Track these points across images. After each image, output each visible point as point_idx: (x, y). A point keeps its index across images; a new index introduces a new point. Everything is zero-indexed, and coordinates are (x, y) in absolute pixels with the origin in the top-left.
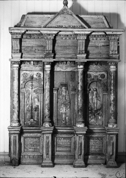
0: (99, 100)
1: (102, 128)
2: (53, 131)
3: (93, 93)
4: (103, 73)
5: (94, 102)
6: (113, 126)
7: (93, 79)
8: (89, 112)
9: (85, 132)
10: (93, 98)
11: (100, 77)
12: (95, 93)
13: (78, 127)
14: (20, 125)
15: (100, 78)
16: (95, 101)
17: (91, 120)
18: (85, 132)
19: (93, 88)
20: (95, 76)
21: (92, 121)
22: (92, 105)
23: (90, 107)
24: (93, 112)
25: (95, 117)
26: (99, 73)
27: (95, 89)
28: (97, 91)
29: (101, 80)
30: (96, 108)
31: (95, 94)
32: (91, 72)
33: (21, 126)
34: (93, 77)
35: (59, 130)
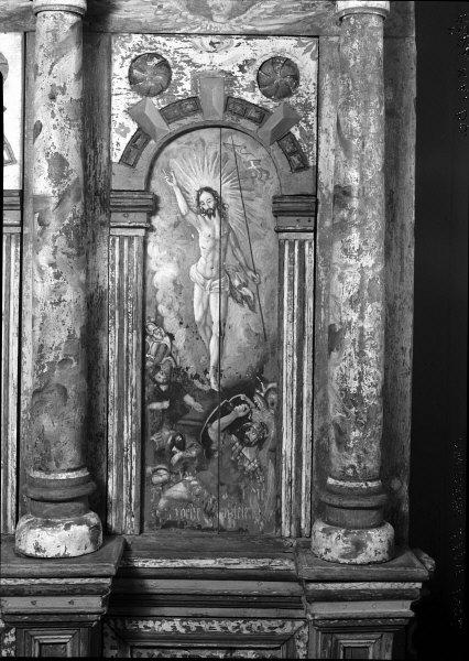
0: (245, 298)
1: (261, 563)
2: (425, 583)
3: (190, 233)
4: (286, 45)
5: (198, 315)
6: (359, 546)
7: (194, 103)
8: (156, 406)
9: (403, 609)
10: (191, 285)
11: (251, 88)
12: (208, 231)
13: (30, 550)
14: (109, 534)
15: (255, 98)
16: (206, 312)
17: (166, 484)
18: (94, 604)
19: (194, 185)
20: (211, 77)
21: (179, 490)
22: (180, 343)
23: (157, 368)
24: (186, 409)
25: (209, 454)
26: (245, 51)
27: (205, 196)
28: (223, 216)
29: (262, 115)
30: (218, 371)
31: (204, 242)
32: (173, 44)
33: (115, 547)
34: (187, 86)
35: (151, 583)
